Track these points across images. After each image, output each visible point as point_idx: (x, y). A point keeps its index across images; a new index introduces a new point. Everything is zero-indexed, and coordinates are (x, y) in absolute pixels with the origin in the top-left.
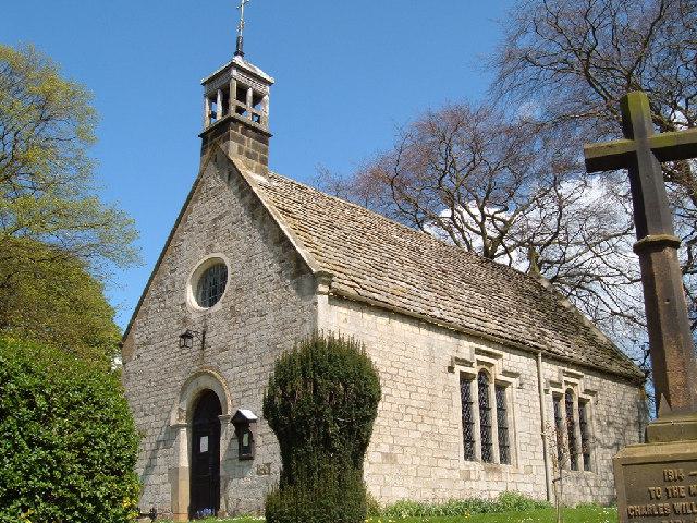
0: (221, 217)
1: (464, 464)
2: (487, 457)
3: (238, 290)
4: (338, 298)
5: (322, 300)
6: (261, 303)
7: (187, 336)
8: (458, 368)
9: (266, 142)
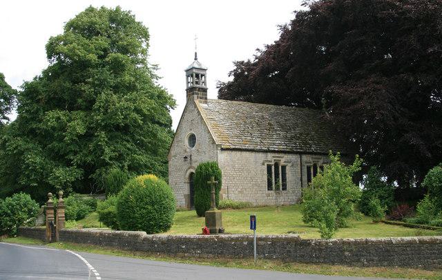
2: (277, 188)
4: (222, 149)
7: (186, 158)
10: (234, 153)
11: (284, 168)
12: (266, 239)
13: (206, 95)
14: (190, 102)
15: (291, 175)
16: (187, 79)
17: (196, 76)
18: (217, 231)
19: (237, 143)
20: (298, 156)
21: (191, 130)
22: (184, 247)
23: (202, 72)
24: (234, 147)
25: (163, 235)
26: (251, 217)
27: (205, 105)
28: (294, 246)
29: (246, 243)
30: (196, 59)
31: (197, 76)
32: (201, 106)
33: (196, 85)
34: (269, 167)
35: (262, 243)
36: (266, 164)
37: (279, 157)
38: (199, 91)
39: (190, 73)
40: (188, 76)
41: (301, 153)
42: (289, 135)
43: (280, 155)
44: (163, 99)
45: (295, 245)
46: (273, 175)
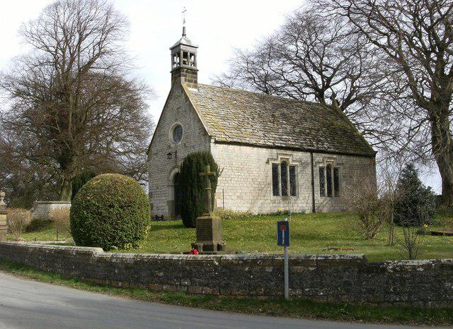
0: (179, 108)
1: (272, 197)
2: (285, 194)
3: (186, 138)
4: (216, 142)
5: (212, 145)
6: (193, 143)
7: (170, 154)
8: (271, 163)
9: (196, 74)
10: (231, 147)
11: (293, 169)
12: (306, 261)
13: (196, 78)
14: (175, 86)
15: (303, 179)
16: (173, 59)
17: (183, 63)
18: (215, 248)
19: (234, 135)
20: (309, 154)
21: (176, 120)
22: (161, 274)
23: (190, 50)
24: (231, 140)
25: (129, 255)
26: (279, 224)
27: (196, 90)
28: (355, 274)
29: (269, 270)
30: (183, 35)
31: (185, 55)
32: (190, 90)
33: (183, 65)
34: (275, 168)
35: (299, 268)
36: (271, 163)
37: (287, 155)
38: (187, 72)
39: (176, 51)
40: (173, 56)
41: (311, 151)
42: (297, 130)
43: (289, 152)
44: (146, 122)
45: (359, 272)
46: (280, 185)
